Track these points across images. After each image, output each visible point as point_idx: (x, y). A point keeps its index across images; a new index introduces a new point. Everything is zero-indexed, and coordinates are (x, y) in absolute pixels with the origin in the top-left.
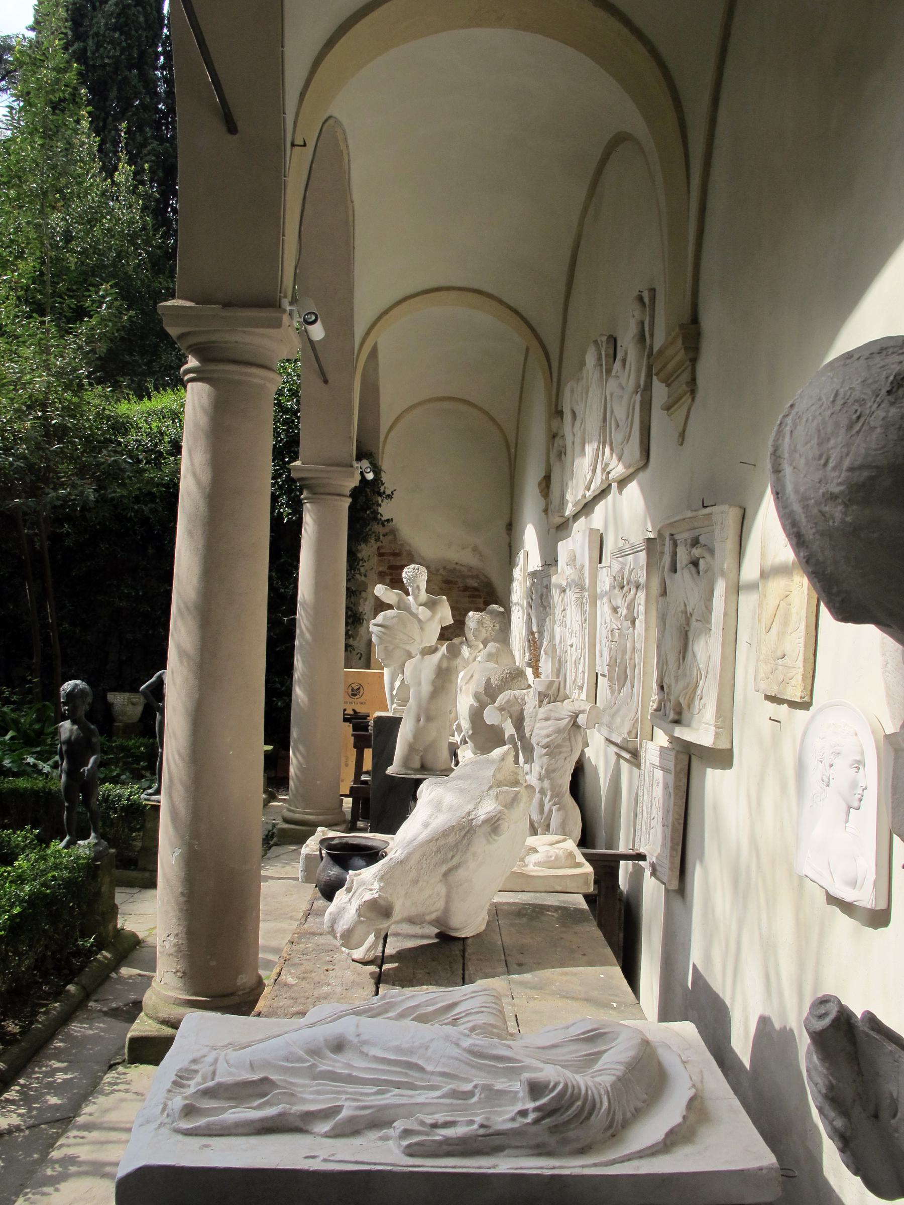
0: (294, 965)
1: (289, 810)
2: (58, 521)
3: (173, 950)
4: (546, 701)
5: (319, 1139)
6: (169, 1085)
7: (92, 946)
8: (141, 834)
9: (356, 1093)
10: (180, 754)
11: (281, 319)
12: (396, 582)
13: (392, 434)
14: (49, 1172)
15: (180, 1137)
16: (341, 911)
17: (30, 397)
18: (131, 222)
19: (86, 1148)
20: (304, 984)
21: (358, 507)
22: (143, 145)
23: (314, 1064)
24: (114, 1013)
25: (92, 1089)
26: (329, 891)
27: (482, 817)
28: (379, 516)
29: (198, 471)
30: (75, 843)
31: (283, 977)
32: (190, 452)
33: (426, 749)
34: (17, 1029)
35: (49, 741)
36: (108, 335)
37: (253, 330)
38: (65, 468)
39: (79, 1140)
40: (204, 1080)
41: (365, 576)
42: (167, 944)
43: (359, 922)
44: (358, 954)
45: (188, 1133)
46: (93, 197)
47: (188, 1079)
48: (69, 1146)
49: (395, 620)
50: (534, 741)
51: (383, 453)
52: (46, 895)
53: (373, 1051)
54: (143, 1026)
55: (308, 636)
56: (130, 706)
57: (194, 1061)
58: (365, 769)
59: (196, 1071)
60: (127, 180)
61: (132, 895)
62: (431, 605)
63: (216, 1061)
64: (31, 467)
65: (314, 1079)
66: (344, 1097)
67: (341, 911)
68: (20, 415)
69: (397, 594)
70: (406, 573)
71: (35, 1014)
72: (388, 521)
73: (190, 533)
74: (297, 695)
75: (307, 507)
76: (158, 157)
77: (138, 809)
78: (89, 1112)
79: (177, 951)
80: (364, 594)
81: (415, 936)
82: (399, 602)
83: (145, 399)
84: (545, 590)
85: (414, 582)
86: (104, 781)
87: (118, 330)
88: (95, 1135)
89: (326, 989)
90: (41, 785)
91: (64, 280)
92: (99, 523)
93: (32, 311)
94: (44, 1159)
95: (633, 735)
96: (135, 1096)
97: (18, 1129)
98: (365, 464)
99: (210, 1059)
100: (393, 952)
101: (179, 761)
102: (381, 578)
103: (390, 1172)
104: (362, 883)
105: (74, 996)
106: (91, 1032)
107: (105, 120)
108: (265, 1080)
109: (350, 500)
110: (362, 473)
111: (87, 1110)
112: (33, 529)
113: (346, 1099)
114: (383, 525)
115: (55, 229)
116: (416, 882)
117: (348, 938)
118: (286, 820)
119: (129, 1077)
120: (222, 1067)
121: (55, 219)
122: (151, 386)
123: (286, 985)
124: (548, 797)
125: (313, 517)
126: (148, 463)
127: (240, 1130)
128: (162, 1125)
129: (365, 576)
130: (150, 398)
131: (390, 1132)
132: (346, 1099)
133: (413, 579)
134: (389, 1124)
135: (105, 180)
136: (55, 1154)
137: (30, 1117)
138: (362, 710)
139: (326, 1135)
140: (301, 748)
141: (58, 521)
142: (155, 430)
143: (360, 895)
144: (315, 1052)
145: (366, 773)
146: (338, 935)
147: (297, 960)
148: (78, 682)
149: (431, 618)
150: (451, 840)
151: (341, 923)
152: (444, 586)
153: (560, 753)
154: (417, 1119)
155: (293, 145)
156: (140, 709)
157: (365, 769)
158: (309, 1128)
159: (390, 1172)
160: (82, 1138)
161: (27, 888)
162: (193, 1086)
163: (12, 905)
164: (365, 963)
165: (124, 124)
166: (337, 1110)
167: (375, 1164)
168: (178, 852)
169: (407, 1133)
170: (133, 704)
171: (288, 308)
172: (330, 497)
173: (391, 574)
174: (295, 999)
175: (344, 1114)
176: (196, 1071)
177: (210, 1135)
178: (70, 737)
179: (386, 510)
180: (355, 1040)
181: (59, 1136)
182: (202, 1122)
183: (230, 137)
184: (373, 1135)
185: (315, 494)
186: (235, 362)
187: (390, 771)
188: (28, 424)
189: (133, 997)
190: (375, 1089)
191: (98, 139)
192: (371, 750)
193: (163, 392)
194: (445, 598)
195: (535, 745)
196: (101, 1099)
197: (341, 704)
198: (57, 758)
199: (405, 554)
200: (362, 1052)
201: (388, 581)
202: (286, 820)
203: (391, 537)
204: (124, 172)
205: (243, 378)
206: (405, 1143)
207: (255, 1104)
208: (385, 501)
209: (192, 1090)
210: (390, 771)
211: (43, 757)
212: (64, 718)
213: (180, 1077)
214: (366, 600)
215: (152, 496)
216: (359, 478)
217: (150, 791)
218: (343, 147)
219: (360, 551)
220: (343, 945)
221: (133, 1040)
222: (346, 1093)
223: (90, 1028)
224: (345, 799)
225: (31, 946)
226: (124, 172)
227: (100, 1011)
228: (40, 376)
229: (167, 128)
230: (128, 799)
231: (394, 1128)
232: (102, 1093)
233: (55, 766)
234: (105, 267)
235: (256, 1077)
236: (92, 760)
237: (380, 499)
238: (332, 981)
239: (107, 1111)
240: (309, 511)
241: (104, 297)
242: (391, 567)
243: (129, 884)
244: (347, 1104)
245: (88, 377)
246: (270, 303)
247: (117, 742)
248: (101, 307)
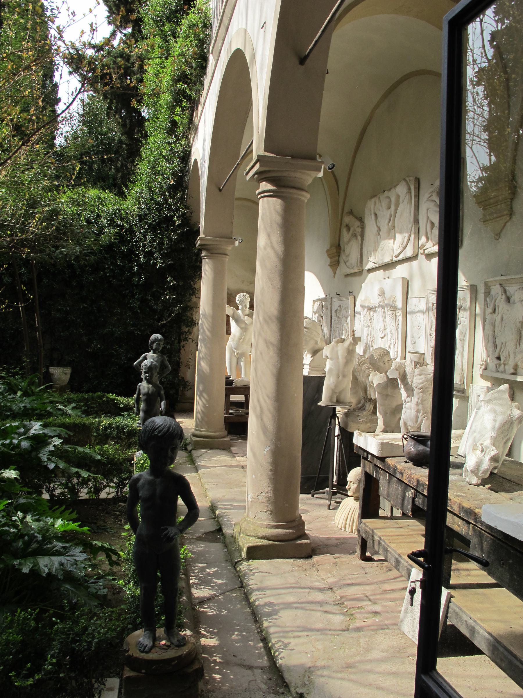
3: (264, 500)
4: (418, 365)
10: (268, 396)
27: (516, 416)
29: (275, 245)
33: (340, 393)
37: (304, 171)
50: (414, 386)
55: (208, 333)
56: (64, 375)
69: (233, 309)
70: (239, 298)
79: (268, 501)
82: (233, 314)
84: (339, 308)
85: (243, 302)
88: (268, 592)
95: (462, 382)
101: (268, 401)
124: (421, 414)
125: (210, 266)
143: (488, 453)
150: (506, 427)
151: (483, 466)
153: (428, 391)
160: (265, 594)
168: (268, 448)
170: (65, 374)
172: (221, 255)
178: (148, 391)
183: (300, 66)
185: (212, 253)
187: (320, 404)
195: (415, 388)
205: (298, 197)
210: (320, 404)
240: (207, 263)
246: (313, 158)
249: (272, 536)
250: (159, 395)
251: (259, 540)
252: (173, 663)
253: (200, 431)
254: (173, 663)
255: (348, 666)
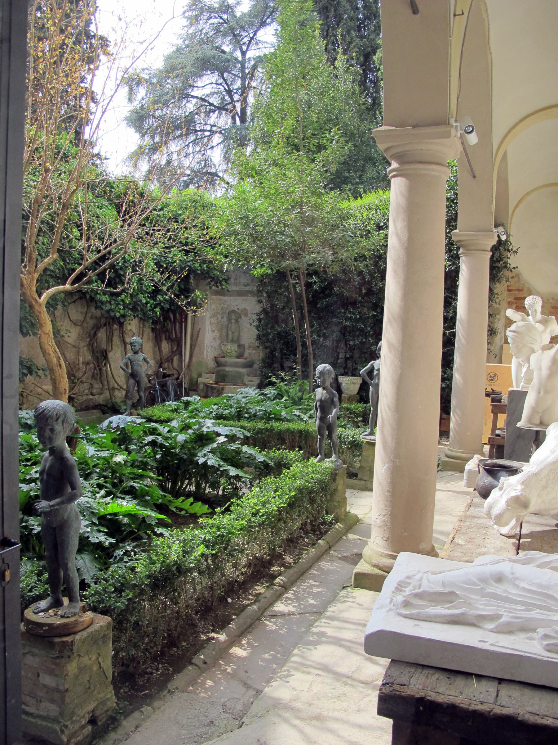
0: (463, 534)
1: (449, 450)
2: (310, 275)
5: (487, 632)
6: (393, 589)
7: (332, 520)
8: (360, 458)
9: (511, 608)
10: (388, 407)
11: (450, 133)
12: (520, 307)
13: (517, 210)
14: (311, 638)
15: (402, 619)
16: (496, 502)
17: (293, 201)
18: (346, 91)
19: (331, 629)
20: (470, 545)
21: (495, 259)
22: (350, 43)
23: (483, 588)
24: (345, 559)
25: (333, 599)
26: (485, 494)
28: (508, 265)
30: (323, 460)
31: (456, 540)
32: (394, 221)
34: (292, 561)
35: (306, 403)
36: (337, 159)
38: (314, 243)
39: (326, 624)
40: (414, 588)
41: (499, 304)
42: (378, 520)
43: (506, 510)
44: (505, 530)
45: (406, 617)
46: (324, 78)
47: (405, 587)
48: (321, 627)
49: (524, 328)
51: (511, 223)
52: (308, 487)
53: (523, 585)
54: (363, 567)
55: (463, 341)
57: (408, 577)
58: (498, 427)
59: (409, 584)
60: (343, 64)
61: (354, 494)
62: (544, 322)
63: (421, 579)
64: (294, 243)
65: (483, 597)
66: (503, 610)
67: (496, 502)
68: (288, 211)
71: (301, 554)
72: (514, 268)
73: (395, 272)
74: (456, 378)
75: (463, 259)
76: (360, 49)
77: (358, 444)
78: (332, 610)
80: (498, 316)
81: (541, 524)
83: (359, 199)
86: (339, 427)
87: (343, 156)
88: (335, 623)
89: (484, 550)
90: (303, 427)
91: (310, 129)
92: (333, 275)
93: (292, 149)
94: (308, 631)
96: (358, 606)
97: (293, 614)
98: (501, 229)
99: (418, 577)
100: (527, 532)
102: (510, 305)
103: (535, 659)
104: (510, 485)
105: (322, 546)
106: (332, 568)
107: (327, 31)
108: (452, 593)
109: (491, 253)
110: (499, 236)
111: (331, 609)
112: (295, 280)
113: (505, 611)
114: (511, 271)
115: (302, 101)
116: (545, 487)
117: (499, 519)
118: (447, 456)
119: (354, 595)
120: (425, 583)
121: (302, 94)
122: (362, 191)
123: (458, 544)
126: (362, 237)
127: (438, 620)
128: (390, 610)
129: (499, 304)
130: (361, 198)
131: (535, 635)
132: (505, 611)
133: (532, 306)
134: (534, 630)
135: (330, 67)
136: (314, 630)
137: (300, 608)
138: (497, 389)
139: (492, 631)
140: (458, 411)
141: (310, 275)
142: (365, 217)
144: (483, 580)
145: (499, 429)
146: (493, 517)
147: (464, 531)
148: (326, 365)
149: (544, 331)
152: (552, 310)
154: (553, 629)
155: (455, 15)
156: (358, 386)
157: (498, 427)
158: (480, 624)
159: (535, 659)
161: (298, 482)
162: (408, 591)
163: (290, 491)
164: (509, 537)
165: (340, 31)
166: (499, 616)
167: (525, 652)
169: (546, 636)
171: (454, 125)
173: (516, 303)
174: (465, 553)
175: (504, 619)
176: (409, 584)
177: (419, 620)
179: (513, 261)
180: (510, 576)
181: (315, 621)
182: (414, 611)
183: (414, 16)
184: (523, 635)
185: (468, 250)
186: (421, 162)
187: (519, 425)
188: (293, 216)
189: (355, 551)
190: (524, 608)
191: (325, 42)
192: (505, 415)
193: (369, 194)
194: (554, 317)
196: (339, 605)
197: (484, 386)
198: (312, 412)
199: (525, 289)
200: (515, 584)
201: (514, 307)
202: (447, 456)
203: (516, 279)
204: (341, 57)
206: (545, 643)
207: (446, 606)
208: (513, 255)
209: (407, 593)
210: (519, 425)
211: (305, 411)
212: (319, 386)
213: (400, 585)
214: (499, 320)
215: (364, 257)
216: (497, 239)
217: (365, 433)
218: (485, 16)
219: (496, 288)
220: (495, 523)
221: (357, 574)
222: (505, 607)
223: (331, 566)
224: (485, 446)
225: (299, 516)
226: (341, 57)
227: (337, 556)
228: (298, 188)
229: (365, 29)
230: (353, 437)
231: (538, 633)
232: (339, 601)
233: (311, 417)
234: (331, 120)
235: (447, 590)
236: (334, 411)
237: (509, 254)
238: (487, 545)
239: (342, 611)
240: (464, 262)
241: (333, 136)
242: (516, 299)
243: (352, 487)
244: (505, 614)
245: (325, 188)
246: (445, 123)
247: (345, 405)
248: (331, 142)
249: (385, 566)
250: (332, 402)
251: (372, 568)
252: (44, 628)
253: (452, 451)
254: (44, 628)
255: (318, 718)
